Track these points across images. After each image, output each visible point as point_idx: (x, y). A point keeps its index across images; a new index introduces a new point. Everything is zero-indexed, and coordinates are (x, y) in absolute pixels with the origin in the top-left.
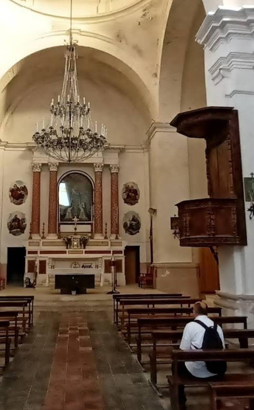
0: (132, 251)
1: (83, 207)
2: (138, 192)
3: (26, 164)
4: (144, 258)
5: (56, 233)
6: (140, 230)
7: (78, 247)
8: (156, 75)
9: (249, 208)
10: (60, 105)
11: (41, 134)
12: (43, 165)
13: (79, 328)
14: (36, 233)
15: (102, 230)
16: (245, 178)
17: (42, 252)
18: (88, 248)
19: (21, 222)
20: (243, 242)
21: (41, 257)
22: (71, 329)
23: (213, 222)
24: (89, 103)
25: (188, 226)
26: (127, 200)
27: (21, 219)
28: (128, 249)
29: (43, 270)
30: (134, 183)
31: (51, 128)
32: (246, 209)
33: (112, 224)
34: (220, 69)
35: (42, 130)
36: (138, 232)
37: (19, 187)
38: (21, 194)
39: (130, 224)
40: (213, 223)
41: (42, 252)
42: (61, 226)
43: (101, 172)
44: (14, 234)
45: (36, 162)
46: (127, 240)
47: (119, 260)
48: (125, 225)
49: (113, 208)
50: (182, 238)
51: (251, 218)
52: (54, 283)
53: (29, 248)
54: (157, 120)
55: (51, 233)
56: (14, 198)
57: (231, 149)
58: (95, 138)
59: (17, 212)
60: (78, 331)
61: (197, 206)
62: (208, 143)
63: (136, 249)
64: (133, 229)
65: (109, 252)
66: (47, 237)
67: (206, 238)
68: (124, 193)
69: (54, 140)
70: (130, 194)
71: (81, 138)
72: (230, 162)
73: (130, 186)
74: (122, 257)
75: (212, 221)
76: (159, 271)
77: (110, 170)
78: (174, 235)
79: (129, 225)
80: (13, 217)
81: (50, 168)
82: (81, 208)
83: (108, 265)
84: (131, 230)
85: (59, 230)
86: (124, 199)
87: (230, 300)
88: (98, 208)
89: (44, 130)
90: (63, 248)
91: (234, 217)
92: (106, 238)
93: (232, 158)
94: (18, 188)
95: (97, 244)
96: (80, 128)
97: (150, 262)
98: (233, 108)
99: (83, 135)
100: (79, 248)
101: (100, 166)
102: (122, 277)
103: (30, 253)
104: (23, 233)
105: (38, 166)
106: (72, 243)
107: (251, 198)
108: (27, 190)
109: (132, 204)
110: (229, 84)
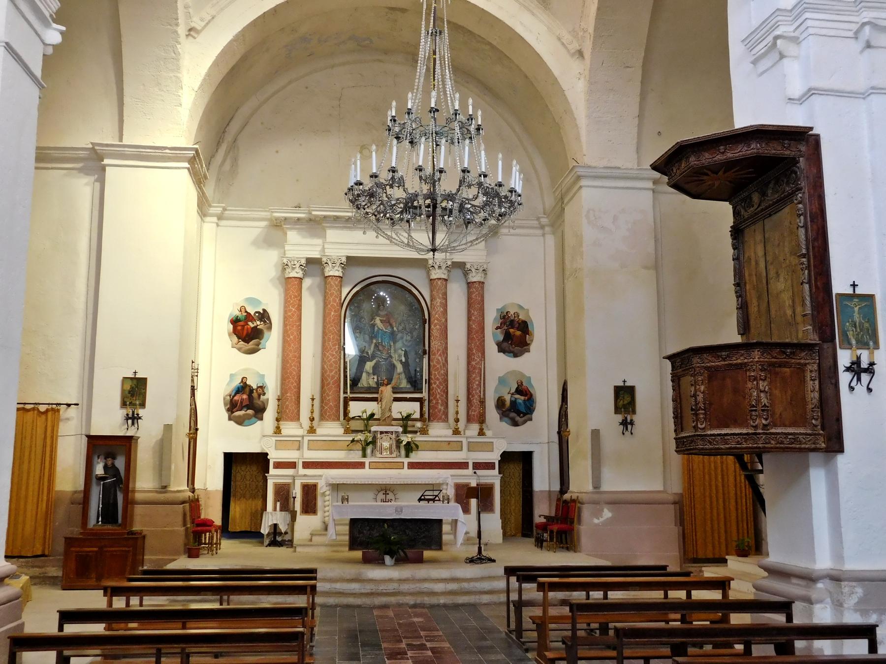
0: (519, 463)
1: (401, 361)
3: (268, 261)
4: (544, 479)
5: (338, 419)
6: (535, 415)
8: (580, 53)
9: (848, 365)
10: (413, 117)
11: (368, 184)
12: (310, 261)
13: (429, 645)
14: (292, 420)
15: (446, 414)
16: (837, 294)
17: (307, 465)
19: (255, 395)
20: (834, 443)
21: (305, 476)
22: (411, 646)
23: (755, 400)
24: (480, 113)
25: (702, 406)
26: (505, 345)
27: (255, 387)
28: (507, 457)
29: (310, 507)
30: (521, 307)
31: (393, 170)
32: (841, 368)
33: (469, 401)
34: (776, 38)
35: (371, 176)
36: (531, 419)
37: (252, 314)
38: (256, 327)
40: (764, 401)
41: (307, 465)
42: (351, 403)
43: (446, 280)
44: (240, 422)
45: (289, 254)
47: (486, 484)
48: (500, 403)
49: (474, 363)
50: (683, 435)
51: (852, 389)
52: (347, 538)
53: (274, 456)
54: (587, 160)
56: (239, 338)
57: (805, 226)
58: (497, 195)
60: (429, 653)
61: (724, 360)
62: (736, 213)
63: (526, 458)
64: (519, 413)
65: (463, 465)
67: (747, 434)
68: (497, 329)
69: (398, 199)
70: (511, 330)
71: (465, 195)
72: (804, 256)
74: (493, 477)
75: (762, 395)
76: (586, 513)
77: (466, 273)
78: (622, 427)
79: (508, 403)
80: (237, 382)
81: (327, 269)
82: (395, 362)
83: (464, 494)
84: (513, 415)
85: (346, 413)
87: (794, 581)
88: (438, 362)
89: (374, 176)
91: (812, 387)
92: (456, 432)
93: (807, 249)
95: (436, 446)
96: (463, 171)
97: (557, 487)
98: (811, 129)
99: (469, 186)
100: (394, 455)
101: (443, 267)
102: (493, 522)
103: (278, 465)
104: (262, 419)
105: (298, 265)
106: (379, 444)
107: (854, 342)
109: (516, 355)
110: (794, 76)
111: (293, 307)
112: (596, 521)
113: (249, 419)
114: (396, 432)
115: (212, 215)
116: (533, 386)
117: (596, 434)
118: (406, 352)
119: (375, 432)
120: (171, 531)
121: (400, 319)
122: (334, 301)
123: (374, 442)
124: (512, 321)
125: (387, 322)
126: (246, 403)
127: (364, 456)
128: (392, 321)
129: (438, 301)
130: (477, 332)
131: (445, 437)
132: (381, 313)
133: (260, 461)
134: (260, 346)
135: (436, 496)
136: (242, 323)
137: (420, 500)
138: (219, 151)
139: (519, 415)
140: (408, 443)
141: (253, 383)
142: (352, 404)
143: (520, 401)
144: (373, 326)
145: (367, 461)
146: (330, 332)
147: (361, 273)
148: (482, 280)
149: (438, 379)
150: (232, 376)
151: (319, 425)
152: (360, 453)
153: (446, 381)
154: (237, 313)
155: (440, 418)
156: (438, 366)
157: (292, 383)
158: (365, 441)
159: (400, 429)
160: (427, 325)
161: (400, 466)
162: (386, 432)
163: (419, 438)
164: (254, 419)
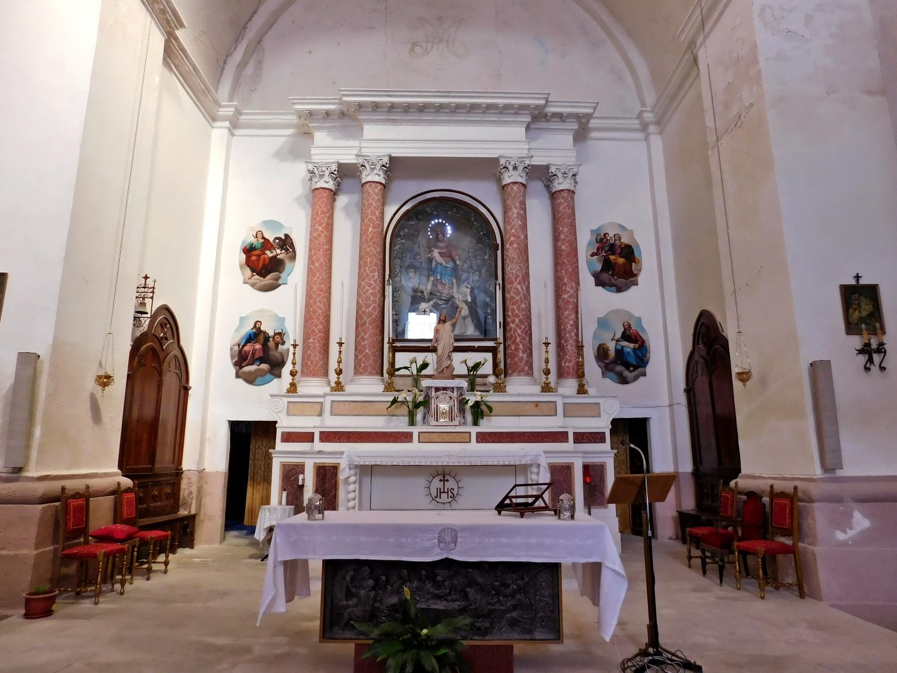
0: (632, 433)
2: (636, 254)
6: (648, 369)
7: (452, 419)
17: (327, 437)
18: (489, 425)
19: (271, 344)
26: (605, 276)
27: (271, 334)
28: (617, 424)
30: (622, 227)
33: (560, 347)
36: (644, 374)
37: (271, 240)
38: (275, 257)
39: (616, 350)
41: (327, 437)
43: (524, 186)
44: (251, 379)
46: (612, 402)
48: (601, 353)
49: (565, 296)
55: (361, 374)
56: (253, 270)
59: (261, 311)
64: (627, 366)
65: (561, 437)
66: (349, 388)
68: (592, 255)
70: (612, 257)
73: (611, 234)
76: (819, 518)
78: (863, 359)
79: (612, 353)
80: (248, 328)
84: (620, 368)
86: (596, 276)
88: (518, 293)
90: (400, 424)
92: (546, 388)
94: (266, 241)
95: (518, 409)
100: (456, 422)
101: (520, 168)
103: (289, 437)
104: (279, 376)
105: (327, 173)
106: (433, 406)
108: (292, 246)
109: (619, 290)
111: (321, 225)
112: (840, 536)
113: (263, 376)
114: (460, 388)
115: (224, 119)
116: (643, 330)
117: (819, 372)
118: (472, 290)
119: (429, 388)
120: (16, 557)
121: (464, 256)
122: (373, 213)
123: (426, 403)
124: (612, 246)
125: (448, 255)
126: (259, 354)
127: (412, 423)
128: (454, 253)
129: (515, 212)
130: (568, 255)
131: (531, 395)
132: (441, 245)
133: (267, 429)
134: (280, 281)
135: (537, 497)
136: (257, 252)
137: (501, 507)
138: (238, 49)
139: (628, 369)
140: (477, 404)
141: (269, 328)
142: (398, 355)
143: (629, 350)
144: (430, 260)
145: (415, 431)
146: (367, 253)
147: (409, 189)
148: (572, 189)
149: (517, 316)
150: (242, 319)
151: (352, 381)
152: (406, 419)
153: (529, 318)
154: (252, 240)
155: (522, 371)
156: (518, 298)
157: (316, 326)
158: (414, 401)
159: (464, 384)
160: (499, 252)
161: (464, 438)
162: (445, 389)
163: (492, 398)
164: (269, 376)
